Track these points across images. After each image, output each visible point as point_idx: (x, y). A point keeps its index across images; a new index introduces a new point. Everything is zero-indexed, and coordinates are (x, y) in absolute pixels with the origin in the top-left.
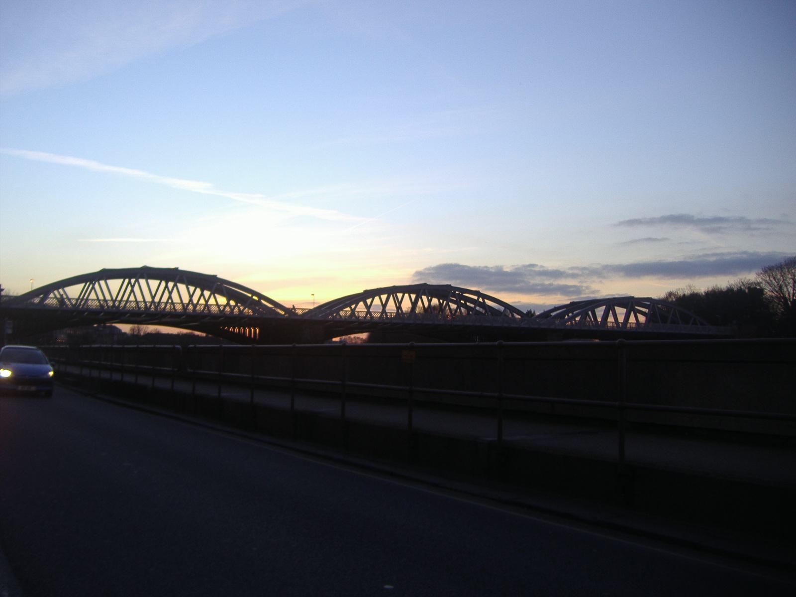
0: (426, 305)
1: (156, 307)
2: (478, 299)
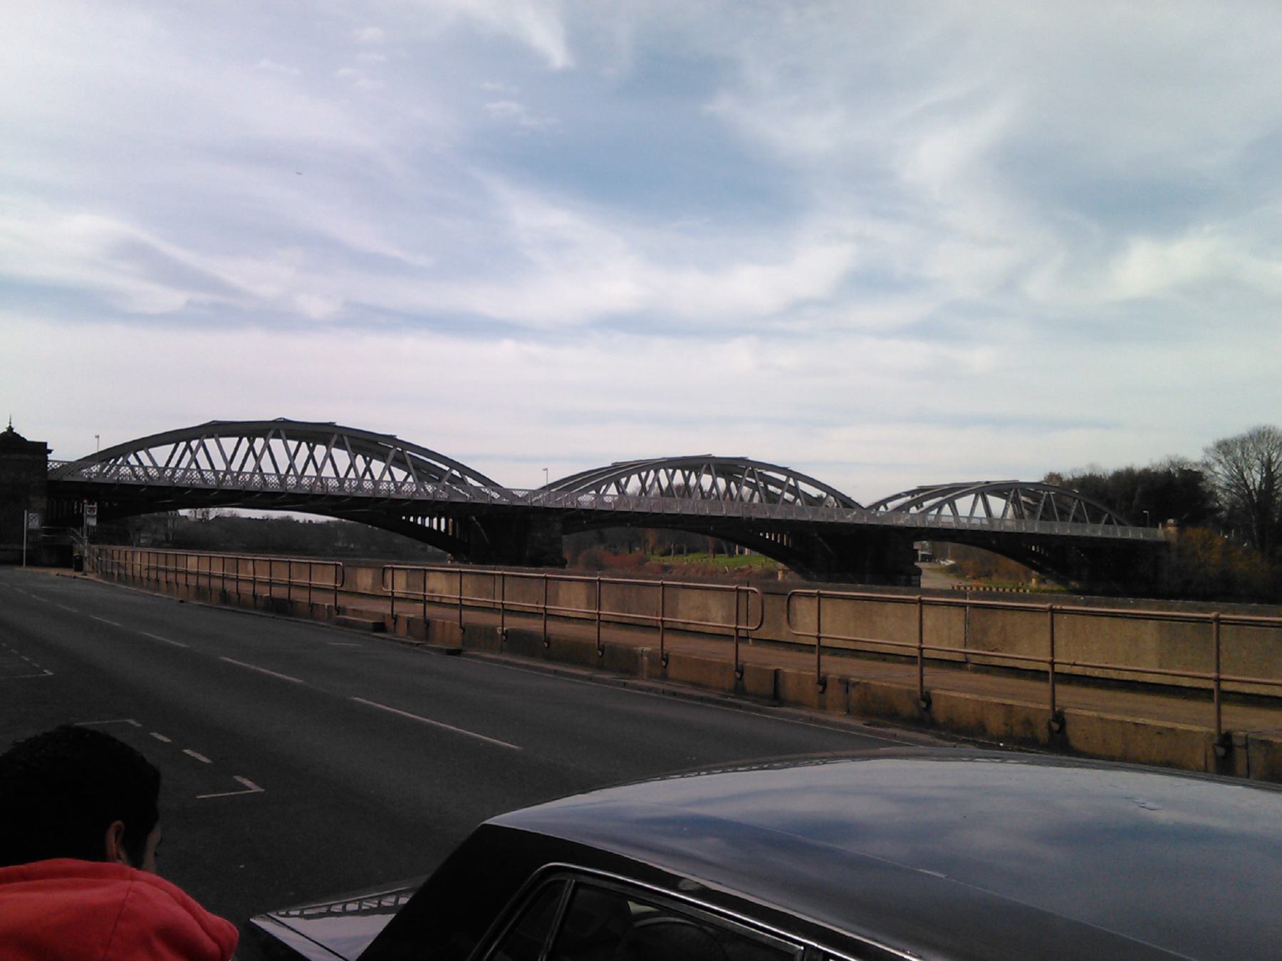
0: (665, 483)
1: (235, 479)
2: (788, 480)
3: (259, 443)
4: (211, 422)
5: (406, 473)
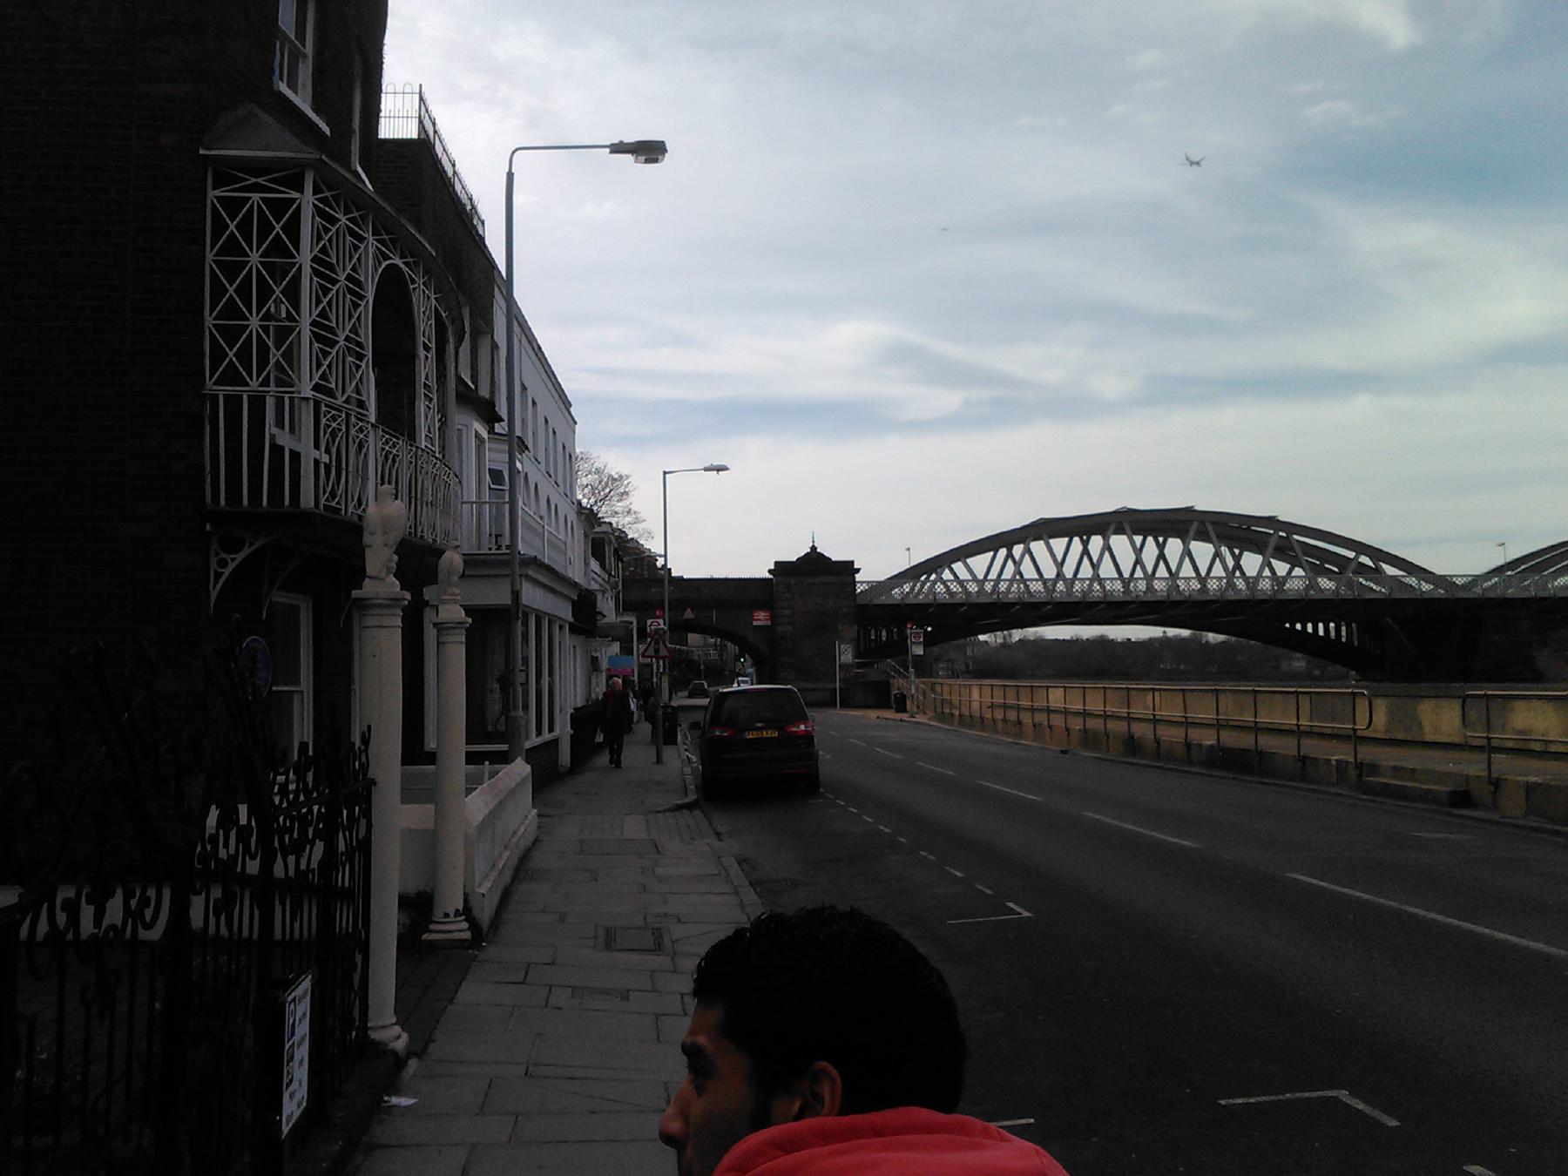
2: (1357, 557)
3: (1018, 550)
4: (1038, 521)
5: (1289, 566)
